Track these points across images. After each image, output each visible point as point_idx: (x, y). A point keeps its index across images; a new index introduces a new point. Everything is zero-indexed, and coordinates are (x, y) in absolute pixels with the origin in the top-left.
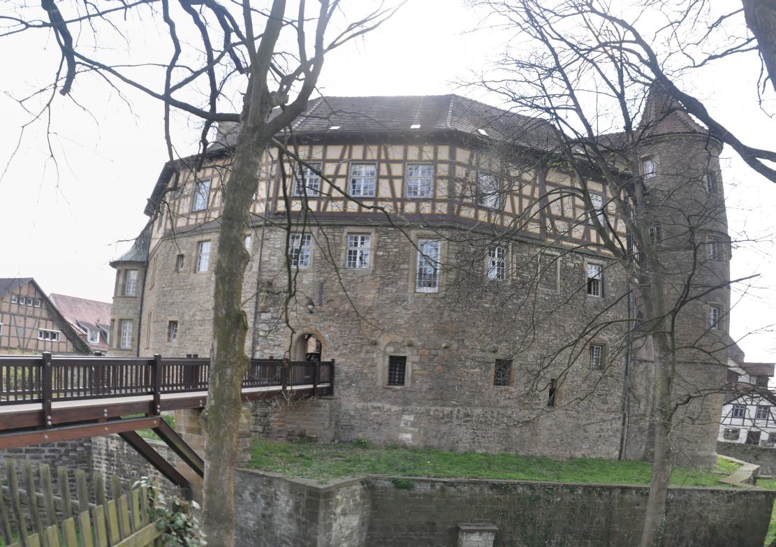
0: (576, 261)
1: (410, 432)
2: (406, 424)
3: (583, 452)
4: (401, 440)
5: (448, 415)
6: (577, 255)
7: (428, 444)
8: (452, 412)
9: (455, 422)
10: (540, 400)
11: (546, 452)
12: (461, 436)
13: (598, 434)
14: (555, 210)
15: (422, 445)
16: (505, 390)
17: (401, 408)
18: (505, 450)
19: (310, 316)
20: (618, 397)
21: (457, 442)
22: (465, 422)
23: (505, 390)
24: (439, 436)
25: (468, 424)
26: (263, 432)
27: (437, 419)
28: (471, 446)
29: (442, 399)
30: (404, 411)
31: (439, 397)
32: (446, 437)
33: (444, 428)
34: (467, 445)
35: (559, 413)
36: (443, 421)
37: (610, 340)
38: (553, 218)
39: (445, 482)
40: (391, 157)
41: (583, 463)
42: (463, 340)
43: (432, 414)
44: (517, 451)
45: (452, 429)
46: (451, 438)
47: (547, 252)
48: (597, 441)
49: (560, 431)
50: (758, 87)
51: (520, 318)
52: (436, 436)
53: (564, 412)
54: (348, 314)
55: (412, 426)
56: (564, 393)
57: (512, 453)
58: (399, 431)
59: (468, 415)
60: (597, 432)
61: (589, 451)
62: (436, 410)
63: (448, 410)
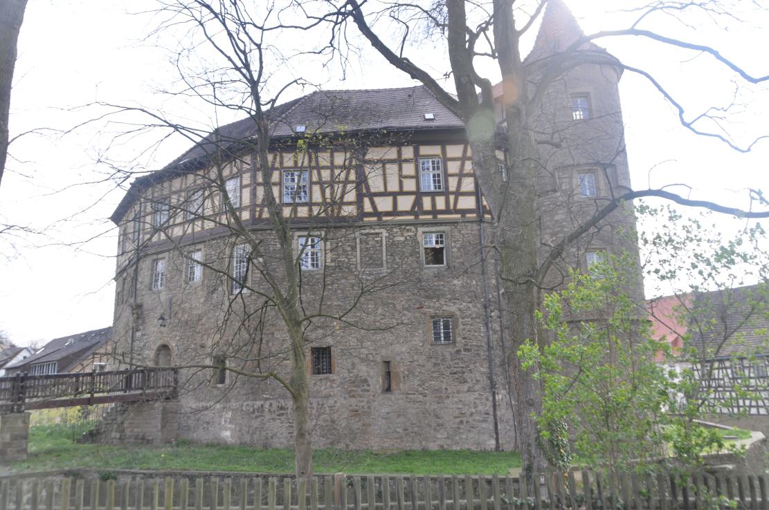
0: (406, 234)
1: (229, 429)
2: (225, 421)
3: (439, 442)
4: (223, 438)
5: (258, 409)
6: (407, 228)
7: (243, 441)
8: (262, 406)
9: (268, 416)
10: (369, 385)
11: (387, 445)
12: (275, 430)
13: (459, 420)
14: (375, 184)
15: (238, 442)
16: (327, 379)
17: (222, 406)
18: (332, 443)
19: (163, 329)
20: (482, 373)
21: (272, 438)
22: (279, 415)
23: (327, 379)
24: (251, 432)
25: (282, 418)
26: (120, 439)
27: (249, 414)
28: (288, 441)
29: (252, 393)
30: (224, 408)
31: (251, 391)
32: (258, 433)
33: (255, 423)
34: (284, 440)
35: (396, 397)
36: (254, 416)
37: (460, 310)
38: (372, 196)
39: (144, 474)
40: (373, 190)
41: (444, 454)
42: (273, 334)
43: (244, 408)
44: (347, 445)
45: (264, 424)
46: (264, 433)
47: (364, 232)
48: (459, 428)
49: (401, 420)
50: (673, 2)
51: (335, 303)
52: (248, 432)
53: (404, 396)
54: (187, 323)
55: (230, 423)
56: (401, 375)
57: (341, 446)
58: (221, 429)
59: (282, 408)
60: (456, 417)
61: (449, 442)
62: (248, 405)
63: (258, 403)
